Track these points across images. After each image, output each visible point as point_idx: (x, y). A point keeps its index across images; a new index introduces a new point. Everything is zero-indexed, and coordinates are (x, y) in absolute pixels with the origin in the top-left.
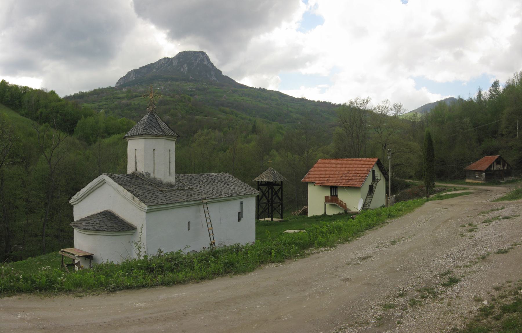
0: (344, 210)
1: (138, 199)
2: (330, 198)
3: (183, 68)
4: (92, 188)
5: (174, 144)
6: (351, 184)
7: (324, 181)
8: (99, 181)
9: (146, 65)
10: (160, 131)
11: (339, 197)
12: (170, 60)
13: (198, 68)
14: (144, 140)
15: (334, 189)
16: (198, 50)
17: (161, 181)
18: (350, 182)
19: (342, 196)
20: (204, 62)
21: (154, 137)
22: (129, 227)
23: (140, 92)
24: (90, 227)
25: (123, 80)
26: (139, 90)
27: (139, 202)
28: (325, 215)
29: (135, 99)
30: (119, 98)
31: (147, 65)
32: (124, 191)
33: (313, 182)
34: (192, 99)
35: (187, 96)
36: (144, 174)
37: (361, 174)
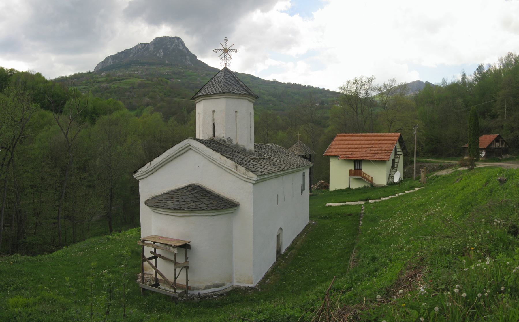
0: (370, 184)
1: (243, 168)
2: (353, 172)
3: (159, 53)
5: (253, 105)
6: (377, 158)
7: (348, 155)
9: (123, 50)
10: (243, 90)
11: (363, 170)
12: (147, 46)
13: (174, 53)
14: (225, 99)
15: (358, 163)
16: (173, 36)
17: (244, 148)
18: (376, 156)
19: (366, 169)
20: (179, 47)
21: (237, 97)
22: (230, 203)
23: (119, 76)
24: (183, 207)
25: (101, 65)
26: (118, 74)
27: (245, 171)
28: (349, 189)
29: (114, 82)
30: (99, 82)
32: (221, 159)
33: (336, 156)
34: (169, 82)
35: (164, 79)
36: (226, 140)
37: (387, 148)
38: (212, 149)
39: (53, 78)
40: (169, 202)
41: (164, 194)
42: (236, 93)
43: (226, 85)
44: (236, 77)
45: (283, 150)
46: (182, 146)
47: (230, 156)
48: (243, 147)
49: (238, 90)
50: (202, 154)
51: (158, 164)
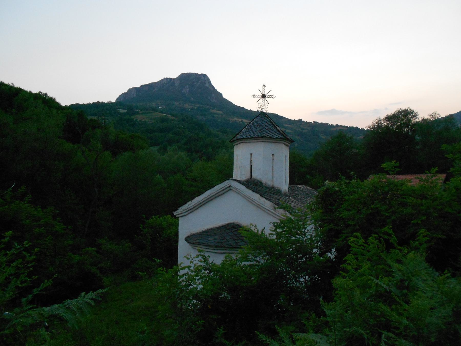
4: (211, 197)
8: (223, 188)
10: (279, 135)
12: (172, 81)
31: (149, 84)
38: (251, 190)
39: (68, 104)
40: (210, 239)
41: (203, 231)
42: (273, 137)
43: (264, 129)
44: (272, 122)
45: (314, 192)
46: (223, 187)
47: (267, 197)
48: (278, 189)
49: (275, 135)
50: (241, 194)
51: (199, 203)
